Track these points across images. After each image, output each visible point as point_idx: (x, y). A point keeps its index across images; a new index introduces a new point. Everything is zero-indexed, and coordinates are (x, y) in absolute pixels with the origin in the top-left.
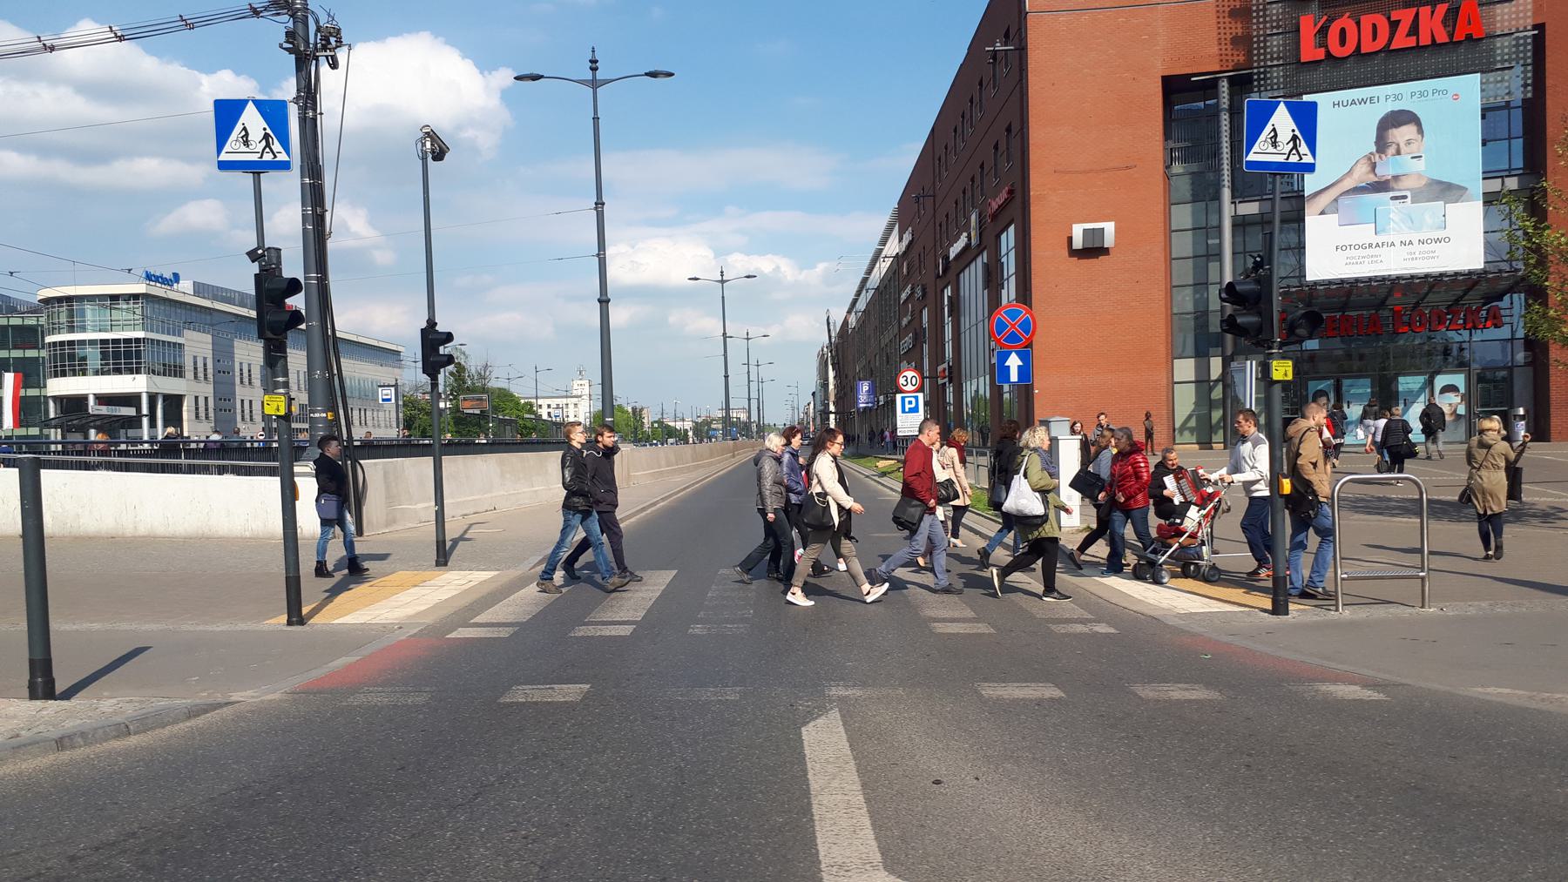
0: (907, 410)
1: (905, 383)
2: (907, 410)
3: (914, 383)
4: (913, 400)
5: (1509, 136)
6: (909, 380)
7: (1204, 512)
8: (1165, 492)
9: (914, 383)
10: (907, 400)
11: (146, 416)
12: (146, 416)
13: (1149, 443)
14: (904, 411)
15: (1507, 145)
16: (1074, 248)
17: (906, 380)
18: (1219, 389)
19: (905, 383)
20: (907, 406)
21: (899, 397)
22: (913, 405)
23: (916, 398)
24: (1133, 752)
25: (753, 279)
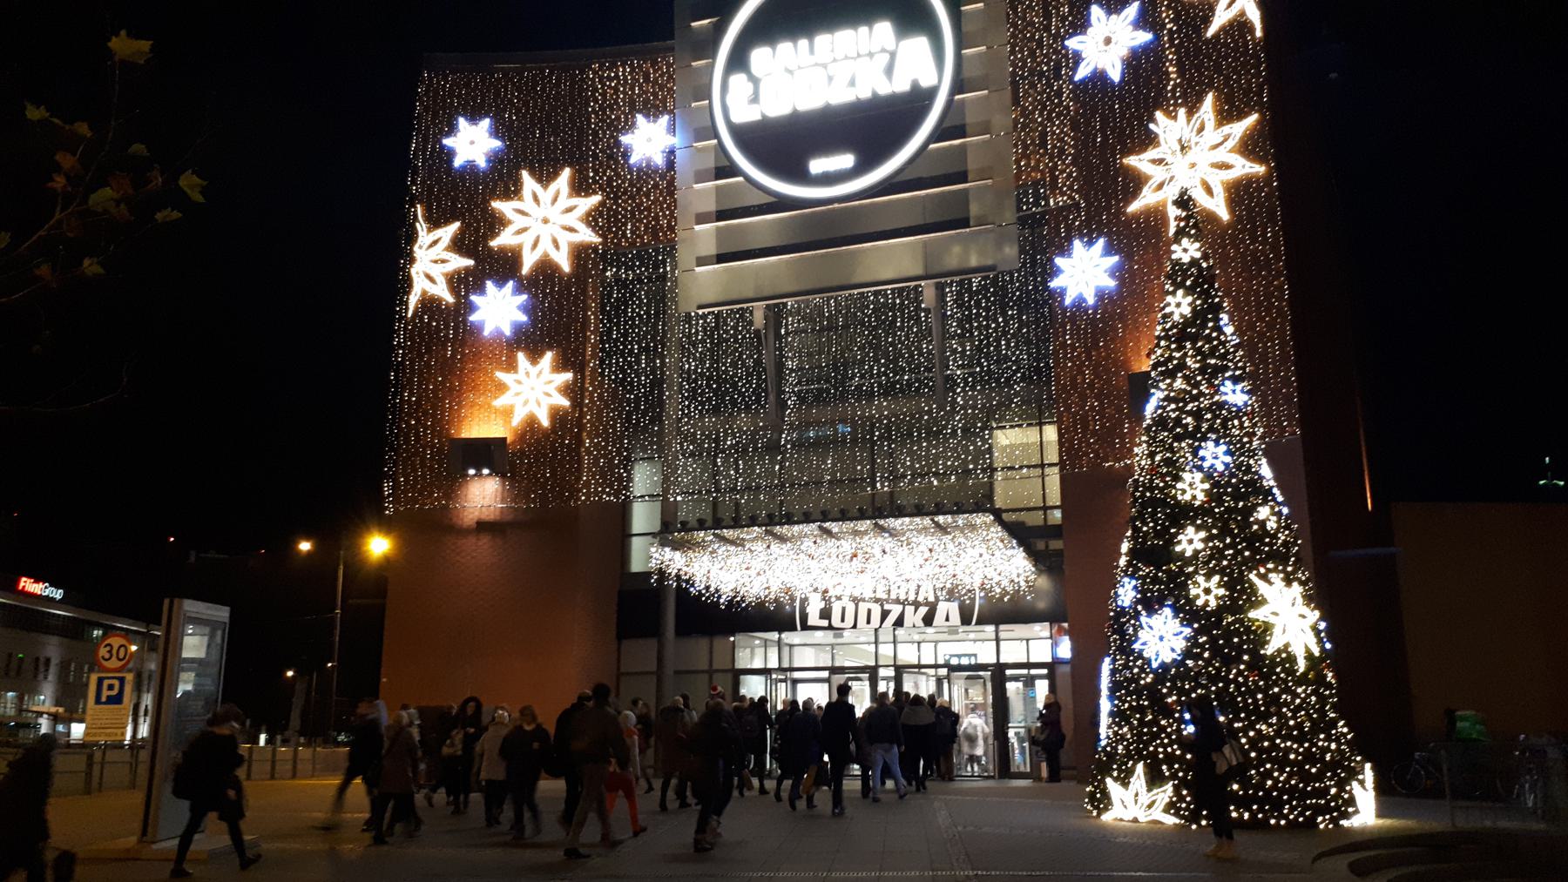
0: (104, 699)
1: (107, 656)
2: (104, 699)
3: (121, 656)
4: (116, 683)
5: (717, 671)
6: (114, 652)
7: (1448, 797)
9: (121, 656)
10: (106, 683)
11: (1047, 547)
12: (1047, 547)
13: (527, 815)
14: (98, 701)
15: (720, 674)
16: (742, 677)
17: (110, 652)
18: (984, 758)
19: (107, 656)
20: (105, 693)
21: (94, 678)
22: (114, 692)
23: (122, 680)
24: (1136, 670)
25: (428, 272)
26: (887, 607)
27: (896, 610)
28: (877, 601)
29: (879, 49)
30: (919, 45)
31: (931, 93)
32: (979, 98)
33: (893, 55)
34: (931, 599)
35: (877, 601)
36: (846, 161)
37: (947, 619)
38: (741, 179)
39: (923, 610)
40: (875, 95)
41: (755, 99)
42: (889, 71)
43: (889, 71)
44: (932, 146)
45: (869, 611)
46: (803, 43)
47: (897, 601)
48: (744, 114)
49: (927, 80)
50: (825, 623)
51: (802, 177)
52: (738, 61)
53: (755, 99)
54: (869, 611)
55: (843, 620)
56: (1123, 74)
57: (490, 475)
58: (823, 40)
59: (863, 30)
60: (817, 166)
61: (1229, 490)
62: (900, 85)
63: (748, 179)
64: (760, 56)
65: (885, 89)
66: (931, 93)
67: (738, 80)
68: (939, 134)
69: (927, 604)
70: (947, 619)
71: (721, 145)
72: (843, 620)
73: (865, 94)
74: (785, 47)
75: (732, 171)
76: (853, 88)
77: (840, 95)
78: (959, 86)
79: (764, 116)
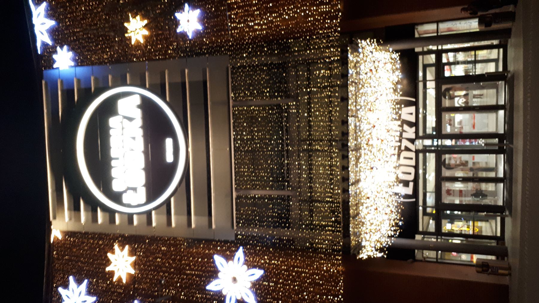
8: (52, 23)
26: (403, 148)
27: (405, 143)
28: (399, 155)
29: (124, 127)
30: (121, 104)
31: (144, 99)
32: (150, 77)
33: (125, 117)
34: (399, 123)
35: (399, 155)
36: (169, 142)
37: (412, 114)
38: (172, 199)
39: (406, 127)
40: (142, 127)
41: (135, 189)
42: (130, 119)
43: (130, 119)
44: (168, 99)
45: (405, 158)
46: (113, 163)
47: (400, 141)
48: (141, 195)
49: (136, 100)
50: (411, 184)
51: (174, 166)
52: (116, 197)
53: (135, 189)
54: (405, 158)
55: (410, 174)
56: (214, 262)
57: (401, 111)
58: (113, 153)
59: (111, 132)
60: (169, 158)
61: (310, 250)
62: (138, 114)
63: (172, 195)
64: (116, 186)
65: (139, 122)
66: (144, 99)
67: (125, 199)
68: (163, 97)
69: (401, 126)
70: (412, 114)
71: (155, 209)
72: (410, 174)
73: (140, 132)
74: (114, 173)
75: (167, 202)
76: (136, 138)
77: (139, 144)
78: (143, 86)
79: (144, 186)
